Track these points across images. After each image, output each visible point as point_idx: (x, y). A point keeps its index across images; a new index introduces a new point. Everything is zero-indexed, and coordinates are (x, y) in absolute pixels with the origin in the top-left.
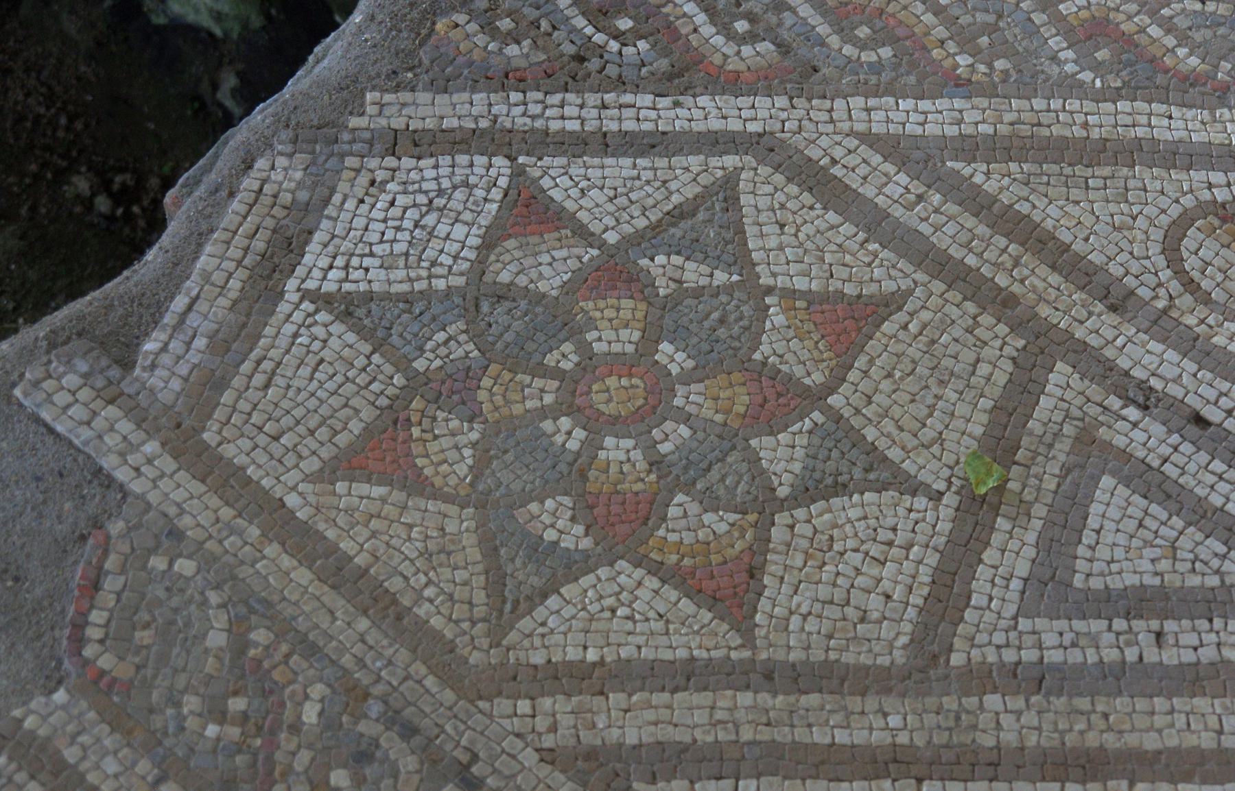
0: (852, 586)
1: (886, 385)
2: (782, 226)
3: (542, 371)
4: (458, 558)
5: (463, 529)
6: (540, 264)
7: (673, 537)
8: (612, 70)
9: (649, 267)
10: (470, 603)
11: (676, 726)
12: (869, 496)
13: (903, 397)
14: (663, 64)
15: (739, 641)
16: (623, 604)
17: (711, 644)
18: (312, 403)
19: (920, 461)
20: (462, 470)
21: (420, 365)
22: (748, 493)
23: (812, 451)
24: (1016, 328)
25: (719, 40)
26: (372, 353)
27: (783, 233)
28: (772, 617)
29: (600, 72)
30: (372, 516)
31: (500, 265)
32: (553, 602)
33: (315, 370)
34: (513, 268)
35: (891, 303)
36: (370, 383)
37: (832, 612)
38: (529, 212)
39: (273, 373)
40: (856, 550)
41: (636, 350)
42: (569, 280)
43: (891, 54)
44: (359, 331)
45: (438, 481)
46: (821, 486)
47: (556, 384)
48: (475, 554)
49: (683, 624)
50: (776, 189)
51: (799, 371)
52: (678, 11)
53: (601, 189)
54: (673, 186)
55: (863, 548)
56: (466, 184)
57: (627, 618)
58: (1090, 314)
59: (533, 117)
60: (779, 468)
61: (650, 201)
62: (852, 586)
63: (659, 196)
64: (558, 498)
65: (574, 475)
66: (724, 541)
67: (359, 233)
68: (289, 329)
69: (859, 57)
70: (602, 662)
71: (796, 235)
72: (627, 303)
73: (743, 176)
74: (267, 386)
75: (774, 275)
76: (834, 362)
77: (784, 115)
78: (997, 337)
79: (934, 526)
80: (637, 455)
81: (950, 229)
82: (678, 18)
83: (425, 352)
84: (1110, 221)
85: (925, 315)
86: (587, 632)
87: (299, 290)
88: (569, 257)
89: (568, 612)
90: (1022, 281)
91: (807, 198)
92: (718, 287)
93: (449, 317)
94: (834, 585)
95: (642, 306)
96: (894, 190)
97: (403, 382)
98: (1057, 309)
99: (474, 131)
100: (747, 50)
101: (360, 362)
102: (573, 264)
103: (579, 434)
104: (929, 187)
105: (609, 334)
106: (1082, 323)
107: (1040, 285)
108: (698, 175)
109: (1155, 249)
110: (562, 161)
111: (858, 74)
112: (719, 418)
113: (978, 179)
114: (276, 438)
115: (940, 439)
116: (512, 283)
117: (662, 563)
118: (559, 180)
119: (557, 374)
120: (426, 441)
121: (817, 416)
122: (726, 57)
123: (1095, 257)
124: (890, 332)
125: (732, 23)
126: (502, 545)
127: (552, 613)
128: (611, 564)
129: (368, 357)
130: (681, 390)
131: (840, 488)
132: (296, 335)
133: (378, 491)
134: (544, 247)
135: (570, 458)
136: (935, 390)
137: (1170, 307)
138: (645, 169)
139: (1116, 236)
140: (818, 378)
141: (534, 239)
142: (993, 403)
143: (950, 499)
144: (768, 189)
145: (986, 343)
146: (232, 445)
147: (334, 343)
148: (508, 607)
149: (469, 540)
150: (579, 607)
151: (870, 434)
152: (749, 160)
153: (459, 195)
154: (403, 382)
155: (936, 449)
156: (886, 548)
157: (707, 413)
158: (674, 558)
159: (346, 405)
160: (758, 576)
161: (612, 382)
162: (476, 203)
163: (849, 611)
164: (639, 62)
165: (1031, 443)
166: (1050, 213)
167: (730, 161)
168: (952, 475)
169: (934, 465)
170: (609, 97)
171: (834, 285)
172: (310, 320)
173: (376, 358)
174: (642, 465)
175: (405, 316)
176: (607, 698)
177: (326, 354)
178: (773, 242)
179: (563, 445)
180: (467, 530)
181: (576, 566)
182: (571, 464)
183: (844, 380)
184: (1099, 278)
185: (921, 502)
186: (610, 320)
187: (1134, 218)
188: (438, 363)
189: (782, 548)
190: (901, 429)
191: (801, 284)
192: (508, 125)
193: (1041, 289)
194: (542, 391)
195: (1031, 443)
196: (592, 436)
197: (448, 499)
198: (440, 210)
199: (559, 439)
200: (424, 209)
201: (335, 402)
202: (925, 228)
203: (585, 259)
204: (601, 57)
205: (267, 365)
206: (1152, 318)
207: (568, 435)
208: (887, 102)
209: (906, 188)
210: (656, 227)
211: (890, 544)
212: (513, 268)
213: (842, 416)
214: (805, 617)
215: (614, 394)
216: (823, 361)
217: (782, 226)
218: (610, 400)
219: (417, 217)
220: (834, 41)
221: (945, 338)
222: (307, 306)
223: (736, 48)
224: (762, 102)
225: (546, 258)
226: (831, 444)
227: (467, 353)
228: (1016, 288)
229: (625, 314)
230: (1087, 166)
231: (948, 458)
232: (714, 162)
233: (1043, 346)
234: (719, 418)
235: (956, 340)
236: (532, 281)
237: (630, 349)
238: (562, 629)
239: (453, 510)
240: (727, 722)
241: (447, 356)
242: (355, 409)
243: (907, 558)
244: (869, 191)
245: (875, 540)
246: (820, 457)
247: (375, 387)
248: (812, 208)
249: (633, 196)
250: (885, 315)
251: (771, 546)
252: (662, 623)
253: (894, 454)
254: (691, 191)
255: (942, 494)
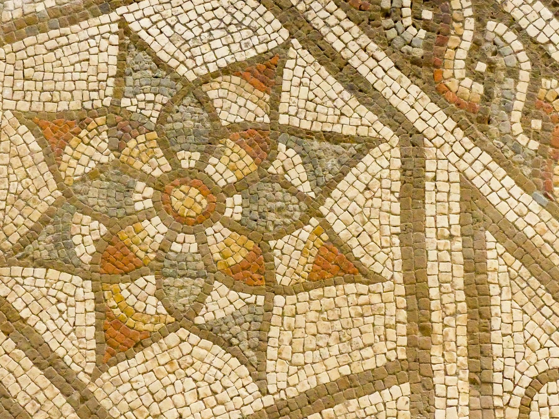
0: (171, 396)
1: (312, 316)
2: (367, 188)
3: (170, 155)
4: (27, 211)
5: (45, 199)
6: (236, 103)
7: (125, 293)
8: (392, 33)
9: (281, 150)
10: (8, 237)
11: (17, 382)
12: (235, 362)
13: (312, 329)
14: (418, 53)
15: (91, 371)
16: (66, 303)
17: (77, 361)
18: (59, 77)
19: (279, 368)
20: (80, 170)
21: (125, 102)
22: (184, 305)
23: (237, 314)
24: (411, 345)
25: (461, 64)
26: (113, 77)
27: (362, 193)
28: (119, 374)
29: (385, 29)
30: (18, 155)
31: (218, 86)
32: (40, 272)
33: (80, 62)
34: (222, 93)
35: (371, 278)
36: (94, 90)
37: (148, 399)
38: (265, 72)
39: (61, 47)
40: (195, 381)
41: (224, 187)
42: (239, 123)
43: (536, 148)
44: (121, 59)
45: (63, 166)
46: (220, 335)
47: (169, 168)
48: (36, 216)
49: (78, 338)
50: (388, 167)
51: (281, 269)
52: (460, 32)
53: (310, 90)
54: (344, 120)
55: (200, 383)
56: (255, 31)
57: (60, 311)
58: (457, 374)
59: (326, 24)
60: (212, 307)
61: (323, 118)
62: (171, 396)
63: (330, 119)
64: (101, 225)
65: (118, 219)
66: (145, 317)
67: (182, 11)
68: (93, 31)
69: (517, 136)
70: (24, 321)
71: (367, 200)
72: (248, 159)
73: (381, 146)
74: (51, 50)
75: (331, 210)
76: (303, 280)
77: (442, 131)
78: (396, 342)
79: (244, 405)
80: (159, 238)
81: (444, 267)
82: (456, 34)
83: (135, 97)
84: (527, 338)
85: (375, 299)
86: (36, 300)
87: (122, 15)
88: (253, 112)
89: (41, 283)
90: (445, 326)
91: (397, 186)
92: (299, 191)
93: (166, 91)
94: (165, 387)
95: (254, 168)
96: (443, 221)
97: (108, 104)
98: (443, 356)
99: (293, 6)
100: (468, 82)
101: (102, 76)
102: (250, 117)
103: (149, 203)
104: (462, 235)
105: (221, 167)
106: (446, 374)
107: (451, 336)
108: (362, 125)
109: (533, 372)
110: (311, 59)
111: (505, 144)
112: (217, 256)
113: (491, 254)
114: (25, 79)
115: (301, 367)
116: (212, 100)
117: (106, 300)
118: (300, 66)
119: (175, 164)
120: (83, 141)
121: (261, 300)
122: (453, 76)
123: (497, 350)
124: (348, 291)
125: (478, 60)
126: (52, 223)
127: (33, 276)
128: (84, 279)
129: (108, 77)
130: (218, 226)
131: (228, 345)
132: (93, 37)
133: (35, 146)
134: (247, 95)
135: (129, 210)
136: (331, 341)
137: (502, 408)
138: (342, 99)
139: (521, 348)
140: (286, 281)
141: (248, 87)
142: (349, 373)
143: (268, 401)
144: (385, 164)
145: (386, 340)
146: (4, 64)
147: (103, 56)
148: (20, 254)
149: (43, 207)
150: (47, 285)
151: (274, 332)
152: (396, 139)
153: (246, 33)
154: (108, 104)
155: (293, 369)
156: (210, 393)
157: (214, 249)
158: (113, 303)
159: (71, 92)
160: (137, 349)
161: (194, 192)
162: (247, 44)
163: (155, 406)
164: (409, 41)
165: (340, 411)
166: (503, 307)
167: (387, 132)
168: (284, 390)
169: (283, 376)
170: (373, 46)
171: (354, 243)
172: (107, 35)
173: (111, 81)
174: (156, 246)
175: (150, 72)
176: (7, 339)
177: (94, 59)
178: (351, 193)
179: (135, 202)
180: (47, 202)
181: (69, 265)
182: (127, 214)
183: (296, 293)
184: (485, 361)
185: (253, 387)
186: (231, 161)
187: (542, 347)
188: (133, 109)
189: (165, 347)
190: (291, 344)
191: (338, 227)
192: (310, 18)
193: (448, 339)
194: (159, 166)
195: (340, 411)
196: (153, 209)
197: (57, 179)
198: (229, 33)
199: (137, 197)
200: (223, 25)
201: (70, 86)
202: (433, 255)
203: (258, 119)
204: (395, 22)
205: (63, 40)
206: (484, 406)
207: (143, 197)
208: (499, 172)
209: (450, 226)
210: (309, 134)
211: (214, 393)
212: (222, 93)
213: (272, 311)
214: (133, 389)
215: (188, 200)
216: (299, 275)
217: (367, 188)
218: (182, 200)
219: (214, 27)
220: (517, 116)
221: (370, 320)
222: (115, 27)
223: (464, 76)
224: (441, 115)
225: (241, 101)
226: (248, 319)
227: (151, 116)
228: (437, 328)
229: (241, 165)
230: (554, 298)
231: (293, 380)
232: (379, 126)
233: (414, 368)
234: (217, 256)
235: (374, 325)
236: (222, 108)
237: (222, 183)
238: (28, 288)
239: (53, 185)
240: (39, 403)
241: (141, 109)
242: (72, 97)
243: (212, 408)
244: (430, 210)
245: (210, 384)
246: (237, 320)
247: (94, 95)
248: (393, 193)
249: (319, 108)
250: (356, 280)
251: (161, 341)
252: (71, 328)
253: (272, 353)
254: (349, 131)
255: (268, 393)
